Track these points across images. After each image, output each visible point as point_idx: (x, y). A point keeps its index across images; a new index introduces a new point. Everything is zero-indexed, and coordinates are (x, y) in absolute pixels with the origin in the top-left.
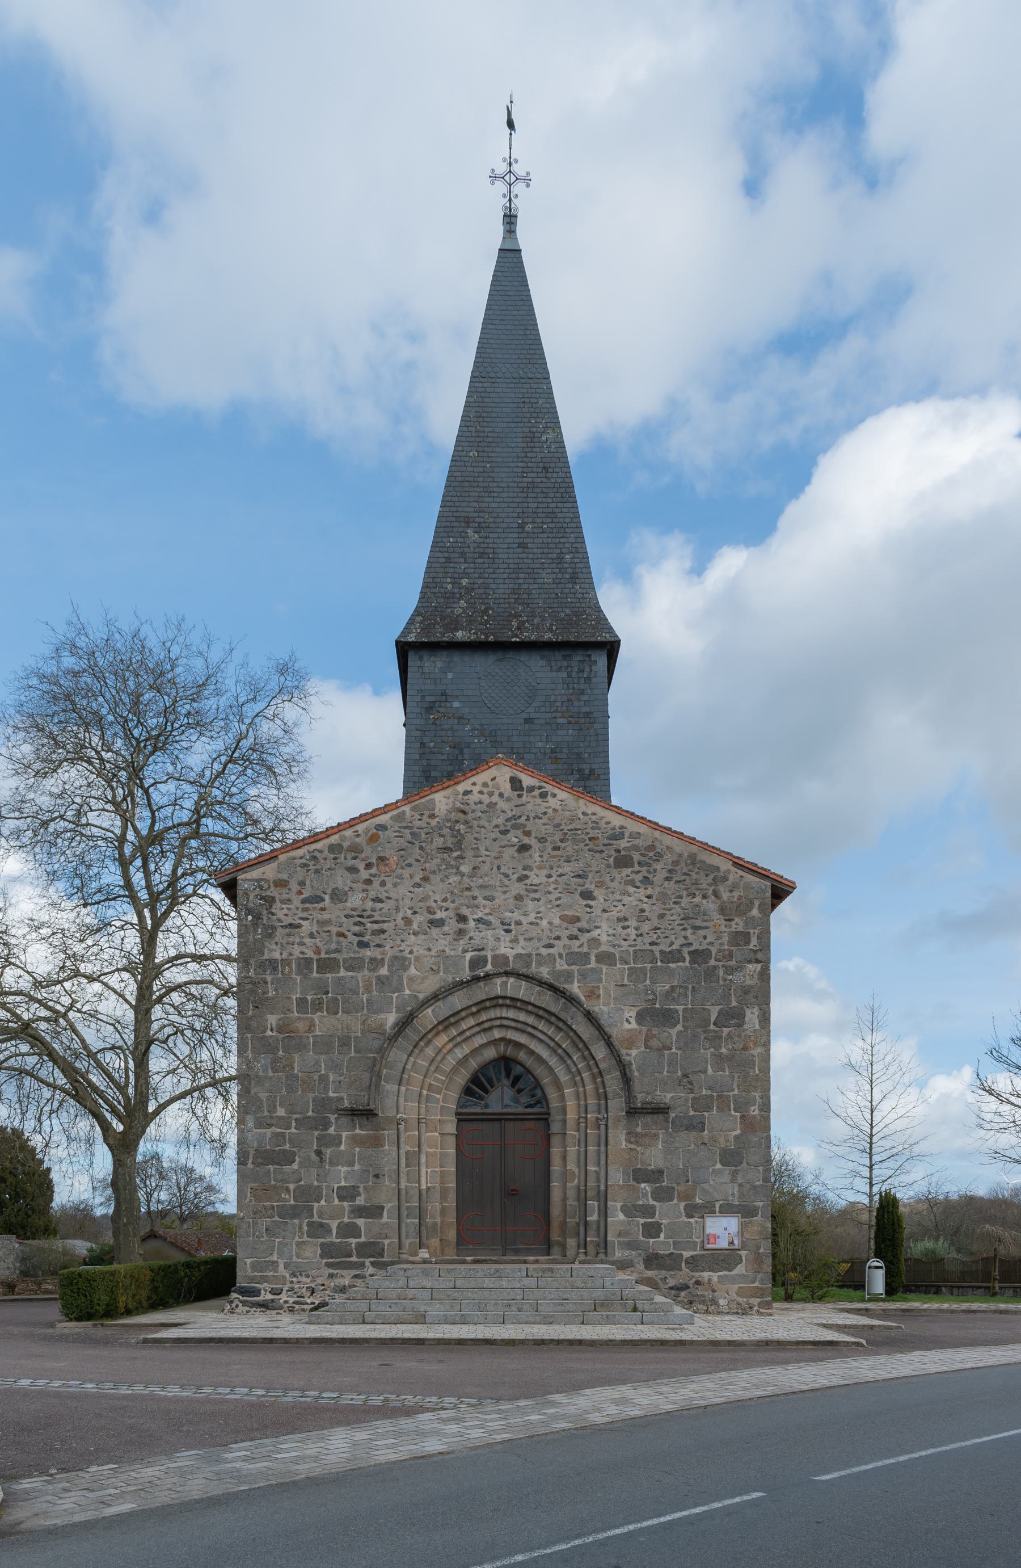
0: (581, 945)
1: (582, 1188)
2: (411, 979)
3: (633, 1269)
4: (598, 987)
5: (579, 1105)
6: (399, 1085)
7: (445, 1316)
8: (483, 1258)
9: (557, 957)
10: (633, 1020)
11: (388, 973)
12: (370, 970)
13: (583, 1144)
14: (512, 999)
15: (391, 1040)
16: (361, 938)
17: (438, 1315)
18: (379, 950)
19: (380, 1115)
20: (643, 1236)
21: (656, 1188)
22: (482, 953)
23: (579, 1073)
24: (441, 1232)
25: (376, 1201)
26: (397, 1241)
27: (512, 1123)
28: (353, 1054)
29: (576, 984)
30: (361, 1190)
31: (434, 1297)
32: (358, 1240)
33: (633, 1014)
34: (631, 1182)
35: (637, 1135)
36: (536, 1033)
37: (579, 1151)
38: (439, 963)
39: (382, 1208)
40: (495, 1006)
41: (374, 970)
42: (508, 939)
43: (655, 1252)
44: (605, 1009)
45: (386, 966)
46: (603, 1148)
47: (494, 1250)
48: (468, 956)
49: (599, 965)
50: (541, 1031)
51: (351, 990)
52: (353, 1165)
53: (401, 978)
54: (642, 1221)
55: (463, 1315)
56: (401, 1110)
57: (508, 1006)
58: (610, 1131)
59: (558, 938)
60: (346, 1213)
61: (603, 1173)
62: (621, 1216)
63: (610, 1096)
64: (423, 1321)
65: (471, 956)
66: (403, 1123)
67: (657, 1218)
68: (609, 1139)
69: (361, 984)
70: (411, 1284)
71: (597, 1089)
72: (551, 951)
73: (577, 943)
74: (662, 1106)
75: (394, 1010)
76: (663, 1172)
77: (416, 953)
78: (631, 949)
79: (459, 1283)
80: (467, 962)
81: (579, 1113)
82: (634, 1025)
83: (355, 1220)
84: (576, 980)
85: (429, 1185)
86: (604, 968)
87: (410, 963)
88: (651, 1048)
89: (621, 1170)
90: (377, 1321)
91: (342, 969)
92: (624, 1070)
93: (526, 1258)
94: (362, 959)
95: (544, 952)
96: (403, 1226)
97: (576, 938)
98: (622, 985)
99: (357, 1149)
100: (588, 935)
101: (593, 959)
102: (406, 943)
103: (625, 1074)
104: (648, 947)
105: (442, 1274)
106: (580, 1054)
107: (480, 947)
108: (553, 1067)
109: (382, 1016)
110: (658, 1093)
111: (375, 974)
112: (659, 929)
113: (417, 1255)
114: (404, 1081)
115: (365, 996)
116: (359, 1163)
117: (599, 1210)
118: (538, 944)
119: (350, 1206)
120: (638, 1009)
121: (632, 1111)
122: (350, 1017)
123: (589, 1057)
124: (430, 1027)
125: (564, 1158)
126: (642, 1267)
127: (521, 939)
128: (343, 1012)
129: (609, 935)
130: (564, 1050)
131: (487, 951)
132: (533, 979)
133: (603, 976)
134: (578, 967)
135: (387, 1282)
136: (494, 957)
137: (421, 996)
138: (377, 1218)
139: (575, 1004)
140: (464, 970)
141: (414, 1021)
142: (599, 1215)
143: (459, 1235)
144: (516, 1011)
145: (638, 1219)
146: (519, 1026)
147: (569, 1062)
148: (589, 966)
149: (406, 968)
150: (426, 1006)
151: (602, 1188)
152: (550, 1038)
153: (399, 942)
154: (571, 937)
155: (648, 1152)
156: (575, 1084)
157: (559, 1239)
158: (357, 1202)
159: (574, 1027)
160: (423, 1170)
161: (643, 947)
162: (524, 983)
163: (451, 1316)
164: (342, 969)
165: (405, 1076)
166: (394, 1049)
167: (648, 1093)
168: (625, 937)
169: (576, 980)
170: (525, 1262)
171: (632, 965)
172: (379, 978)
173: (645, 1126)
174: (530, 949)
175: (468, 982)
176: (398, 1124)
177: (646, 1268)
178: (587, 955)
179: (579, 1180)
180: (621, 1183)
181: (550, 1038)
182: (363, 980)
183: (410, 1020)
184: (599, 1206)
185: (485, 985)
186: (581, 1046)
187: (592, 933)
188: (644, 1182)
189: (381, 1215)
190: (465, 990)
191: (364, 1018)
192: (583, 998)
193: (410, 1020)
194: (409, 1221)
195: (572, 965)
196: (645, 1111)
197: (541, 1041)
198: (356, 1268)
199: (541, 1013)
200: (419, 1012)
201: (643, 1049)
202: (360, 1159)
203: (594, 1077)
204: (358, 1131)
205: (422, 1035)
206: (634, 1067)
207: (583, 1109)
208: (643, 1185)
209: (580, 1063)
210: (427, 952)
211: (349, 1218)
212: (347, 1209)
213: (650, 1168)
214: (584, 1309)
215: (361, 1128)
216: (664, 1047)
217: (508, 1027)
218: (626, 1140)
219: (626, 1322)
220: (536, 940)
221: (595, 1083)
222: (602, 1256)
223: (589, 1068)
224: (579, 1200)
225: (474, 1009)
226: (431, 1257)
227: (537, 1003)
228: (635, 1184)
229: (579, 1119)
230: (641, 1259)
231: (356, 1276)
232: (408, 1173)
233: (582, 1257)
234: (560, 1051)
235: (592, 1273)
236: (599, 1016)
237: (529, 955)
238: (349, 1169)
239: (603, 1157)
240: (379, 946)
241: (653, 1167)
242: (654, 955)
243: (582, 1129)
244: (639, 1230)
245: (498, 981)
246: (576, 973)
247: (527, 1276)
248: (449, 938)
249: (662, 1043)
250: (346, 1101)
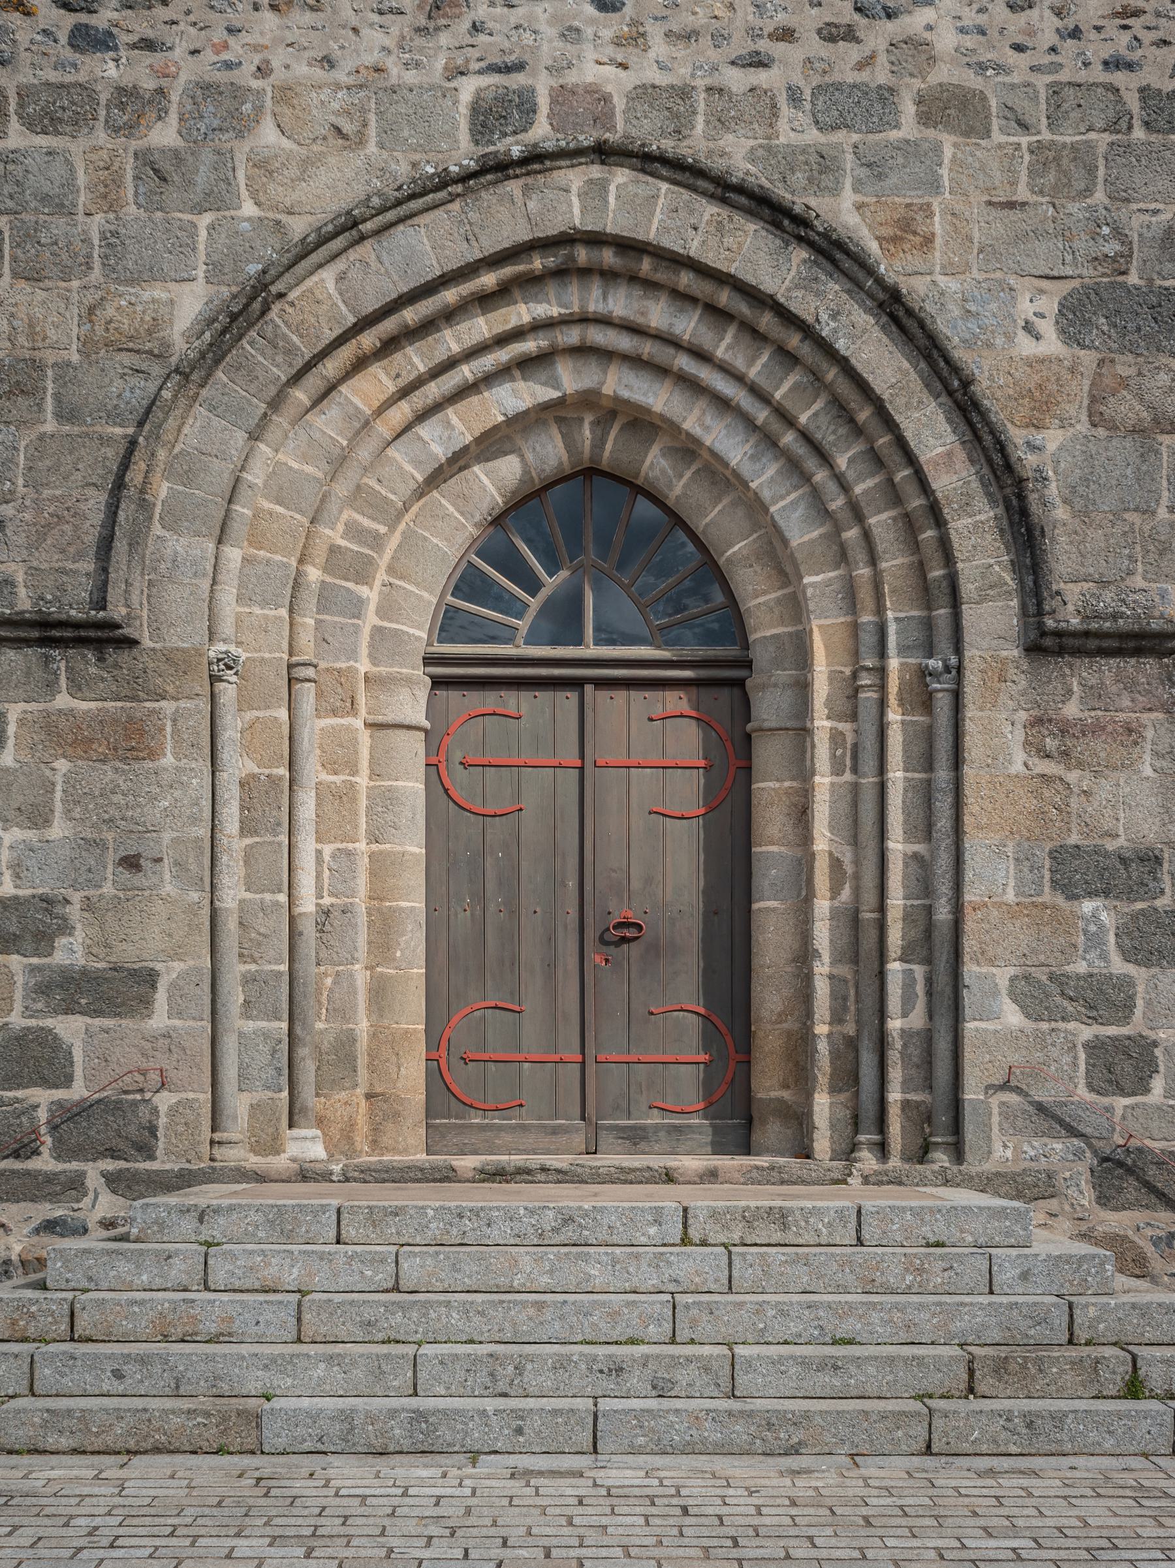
0: (867, 62)
1: (868, 916)
2: (263, 165)
3: (1053, 1204)
4: (927, 210)
5: (855, 627)
6: (220, 541)
7: (347, 1416)
8: (517, 1160)
9: (782, 100)
10: (1047, 328)
11: (179, 143)
12: (115, 130)
13: (869, 763)
14: (628, 246)
15: (186, 376)
16: (83, 18)
17: (314, 1416)
18: (148, 58)
19: (147, 643)
20: (1091, 1088)
21: (1135, 917)
22: (517, 80)
23: (859, 516)
24: (372, 1068)
25: (128, 954)
26: (205, 1097)
27: (620, 695)
28: (50, 426)
29: (848, 197)
30: (74, 912)
31: (308, 1332)
32: (59, 1094)
33: (1050, 305)
34: (1047, 896)
35: (1065, 729)
36: (705, 374)
37: (855, 788)
38: (363, 111)
39: (150, 978)
40: (560, 273)
41: (130, 129)
42: (607, 34)
43: (1134, 1143)
44: (951, 284)
45: (173, 118)
46: (943, 775)
47: (555, 1131)
48: (468, 88)
49: (931, 133)
50: (724, 369)
51: (45, 199)
52: (47, 822)
53: (224, 158)
54: (1087, 1033)
55: (420, 1416)
56: (227, 627)
57: (609, 276)
58: (970, 712)
59: (786, 35)
60: (18, 995)
61: (944, 861)
62: (1013, 1017)
63: (968, 588)
64: (251, 1442)
65: (479, 91)
66: (230, 675)
67: (1136, 1025)
68: (968, 742)
69: (82, 179)
70: (220, 1274)
71: (921, 568)
72: (761, 77)
73: (854, 53)
74: (1155, 625)
75: (200, 273)
76: (1158, 860)
77: (279, 75)
78: (1042, 81)
79: (413, 1269)
80: (464, 110)
81: (856, 654)
82: (1051, 344)
83: (49, 1022)
84: (848, 183)
85: (327, 901)
86: (948, 143)
87: (259, 109)
88: (1112, 427)
89: (1010, 850)
90: (51, 1441)
91: (14, 124)
92: (1021, 497)
93: (672, 1162)
94: (86, 90)
95: (737, 80)
96: (230, 1045)
97: (849, 35)
98: (1011, 205)
99: (62, 765)
100: (890, 26)
101: (909, 109)
102: (245, 37)
103: (1024, 512)
104: (1098, 74)
105: (349, 1232)
106: (858, 448)
107: (510, 59)
108: (766, 494)
109: (158, 292)
110: (1138, 582)
111: (135, 144)
112: (1137, 13)
113: (277, 1152)
114: (238, 528)
115: (99, 218)
116: (68, 813)
117: (929, 994)
118: (713, 55)
119: (33, 969)
120: (1067, 286)
121: (1048, 642)
122: (41, 295)
123: (893, 457)
124: (329, 335)
125: (802, 814)
126: (1086, 1197)
127: (655, 32)
128: (15, 275)
129: (962, 30)
130: (805, 436)
131: (534, 74)
132: (698, 172)
133: (944, 172)
134: (855, 137)
135: (124, 1267)
136: (560, 95)
137: (299, 227)
138: (131, 1013)
139: (847, 264)
140: (451, 135)
141: (273, 314)
142: (931, 1015)
143: (437, 1079)
144: (638, 292)
145: (1072, 1026)
146: (648, 348)
147: (821, 476)
148: (894, 135)
149: (242, 127)
150: (314, 258)
151: (943, 914)
152: (755, 391)
153: (218, 35)
154: (833, 34)
155: (1104, 789)
156: (843, 556)
157: (786, 1095)
158: (59, 958)
159: (841, 345)
160: (307, 846)
161: (1082, 76)
162: (664, 186)
163: (371, 1418)
164: (14, 124)
165: (241, 510)
166: (200, 410)
167: (1103, 583)
168: (1019, 39)
169: (848, 183)
170: (669, 1177)
171: (1046, 136)
172: (145, 158)
173: (1095, 695)
174: (684, 71)
175: (465, 178)
176: (214, 679)
177: (1103, 1200)
178: (886, 96)
179: (857, 891)
180: (1010, 897)
181: (755, 391)
182: (88, 162)
183: (257, 306)
184: (929, 981)
185: (527, 190)
186: (864, 415)
187: (904, 20)
188: (1091, 894)
189: (146, 1003)
190: (456, 206)
191: (91, 298)
192: (873, 247)
193: (257, 306)
194: (250, 1026)
195: (835, 128)
196: (1092, 644)
197: (723, 404)
198: (53, 1198)
199: (724, 297)
200: (288, 278)
201: (1083, 427)
202: (72, 800)
203: (909, 525)
204: (63, 701)
205: (299, 363)
206: (1053, 490)
207: (868, 639)
208: (1088, 906)
209: (861, 478)
210: (318, 73)
211: (28, 1012)
212: (20, 980)
213: (1111, 845)
214: (927, 1385)
215: (76, 688)
216: (1156, 421)
217: (606, 355)
218: (1027, 743)
219: (1109, 1444)
220: (706, 41)
221: (915, 546)
222: (941, 1159)
223: (893, 495)
224: (855, 959)
225: (488, 280)
226: (331, 1155)
227: (711, 258)
228: (1060, 900)
229: (855, 676)
230: (1082, 1168)
231: (50, 1226)
232: (249, 856)
233: (868, 1161)
234: (788, 438)
235: (937, 1229)
236: (930, 307)
237: (684, 93)
238: (31, 835)
239: (943, 805)
240: (148, 45)
241: (1121, 841)
242: (1120, 101)
243: (868, 713)
244: (1075, 1065)
245: (575, 178)
246: (849, 157)
247: (685, 1241)
248: (398, 25)
249: (1151, 407)
250: (22, 592)
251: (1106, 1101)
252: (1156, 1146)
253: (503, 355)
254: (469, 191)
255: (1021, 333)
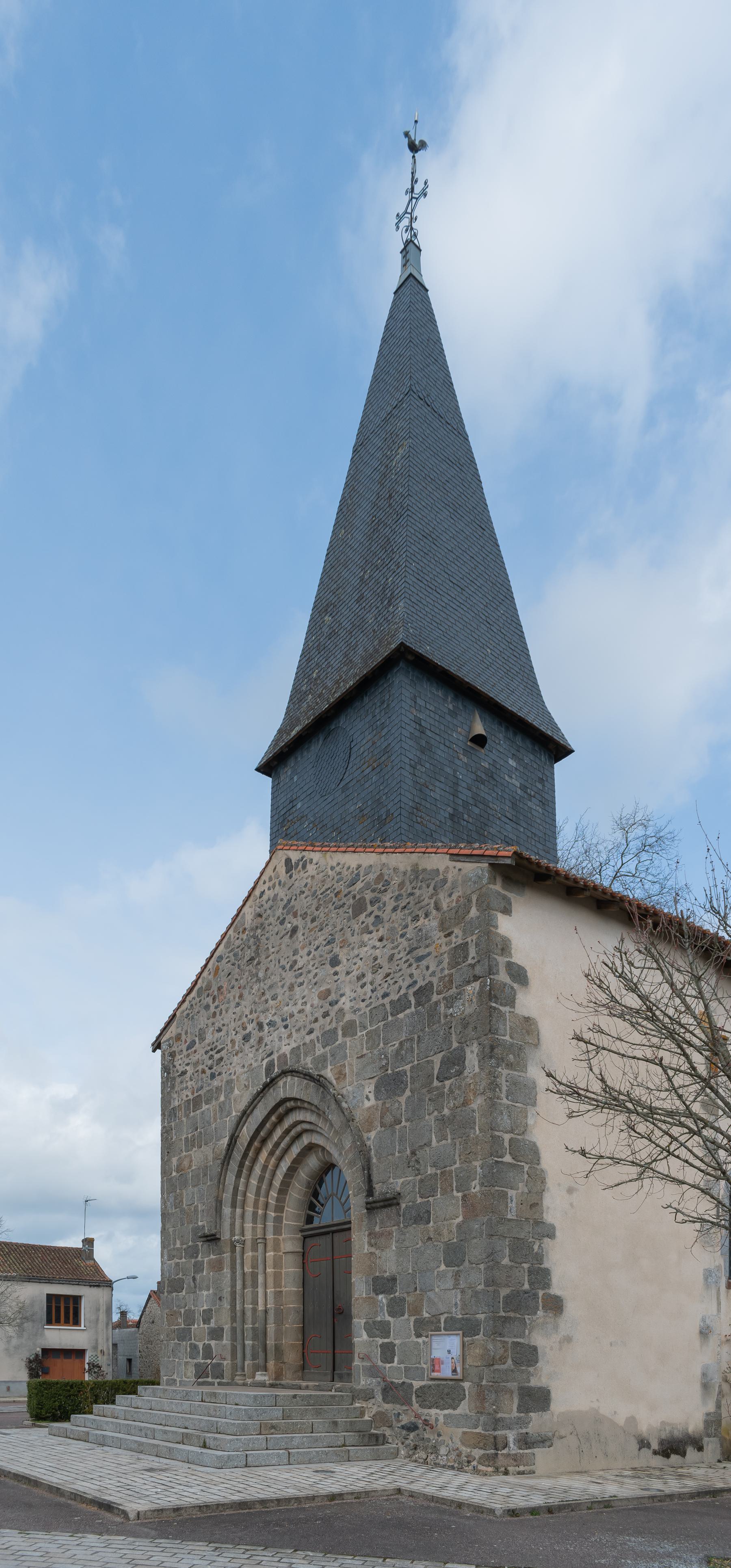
62: (365, 1336)
89: (364, 1279)
150: (241, 1124)
171: (370, 1028)
180: (364, 1296)
201: (379, 1129)
251: (384, 1365)
252: (396, 1381)
253: (287, 1139)
254: (265, 1095)
255: (365, 1100)
